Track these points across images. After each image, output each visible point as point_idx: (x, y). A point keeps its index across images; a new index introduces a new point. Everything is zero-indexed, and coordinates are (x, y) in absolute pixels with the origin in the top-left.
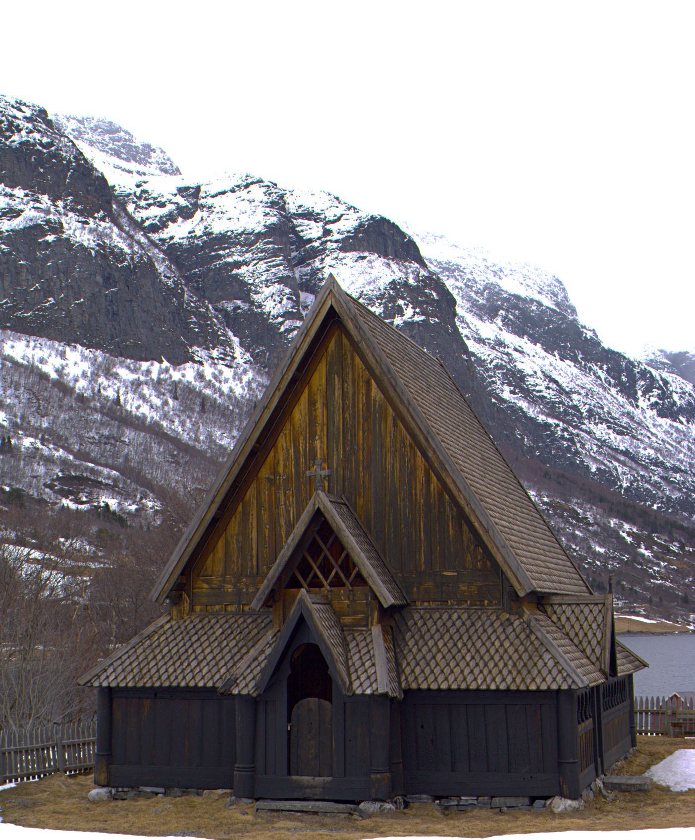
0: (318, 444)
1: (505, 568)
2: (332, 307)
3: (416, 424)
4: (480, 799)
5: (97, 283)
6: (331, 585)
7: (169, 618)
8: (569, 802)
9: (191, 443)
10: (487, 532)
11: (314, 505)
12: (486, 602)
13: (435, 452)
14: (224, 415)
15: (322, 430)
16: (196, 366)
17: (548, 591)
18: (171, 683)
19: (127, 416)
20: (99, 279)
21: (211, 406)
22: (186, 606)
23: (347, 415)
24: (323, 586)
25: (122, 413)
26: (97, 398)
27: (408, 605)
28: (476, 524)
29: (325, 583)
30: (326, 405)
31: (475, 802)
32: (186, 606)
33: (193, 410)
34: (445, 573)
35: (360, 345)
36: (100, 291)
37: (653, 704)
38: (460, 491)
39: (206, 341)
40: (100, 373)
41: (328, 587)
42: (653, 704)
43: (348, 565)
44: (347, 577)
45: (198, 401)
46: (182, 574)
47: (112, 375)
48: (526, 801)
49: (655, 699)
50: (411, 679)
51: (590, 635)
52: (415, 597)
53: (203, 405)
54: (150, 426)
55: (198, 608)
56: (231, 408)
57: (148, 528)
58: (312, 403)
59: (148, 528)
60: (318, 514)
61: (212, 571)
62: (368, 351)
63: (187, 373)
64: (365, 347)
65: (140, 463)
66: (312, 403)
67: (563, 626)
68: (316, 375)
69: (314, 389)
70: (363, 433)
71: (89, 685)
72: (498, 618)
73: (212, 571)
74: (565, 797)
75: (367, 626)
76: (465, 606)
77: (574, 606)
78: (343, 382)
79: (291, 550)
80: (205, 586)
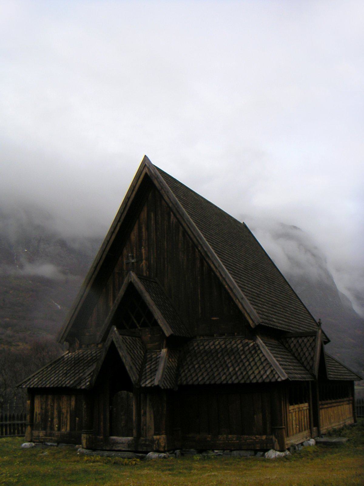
0: (143, 251)
3: (192, 232)
4: (226, 451)
8: (278, 453)
12: (236, 334)
13: (202, 247)
17: (286, 330)
18: (227, 381)
22: (77, 345)
24: (137, 327)
30: (148, 229)
31: (221, 454)
35: (161, 192)
38: (216, 268)
41: (139, 328)
43: (150, 315)
50: (184, 379)
51: (307, 354)
55: (83, 346)
58: (140, 229)
60: (131, 286)
62: (165, 195)
64: (164, 192)
66: (140, 229)
67: (292, 350)
70: (167, 242)
71: (21, 387)
72: (241, 342)
74: (276, 450)
76: (224, 337)
77: (298, 338)
78: (156, 215)
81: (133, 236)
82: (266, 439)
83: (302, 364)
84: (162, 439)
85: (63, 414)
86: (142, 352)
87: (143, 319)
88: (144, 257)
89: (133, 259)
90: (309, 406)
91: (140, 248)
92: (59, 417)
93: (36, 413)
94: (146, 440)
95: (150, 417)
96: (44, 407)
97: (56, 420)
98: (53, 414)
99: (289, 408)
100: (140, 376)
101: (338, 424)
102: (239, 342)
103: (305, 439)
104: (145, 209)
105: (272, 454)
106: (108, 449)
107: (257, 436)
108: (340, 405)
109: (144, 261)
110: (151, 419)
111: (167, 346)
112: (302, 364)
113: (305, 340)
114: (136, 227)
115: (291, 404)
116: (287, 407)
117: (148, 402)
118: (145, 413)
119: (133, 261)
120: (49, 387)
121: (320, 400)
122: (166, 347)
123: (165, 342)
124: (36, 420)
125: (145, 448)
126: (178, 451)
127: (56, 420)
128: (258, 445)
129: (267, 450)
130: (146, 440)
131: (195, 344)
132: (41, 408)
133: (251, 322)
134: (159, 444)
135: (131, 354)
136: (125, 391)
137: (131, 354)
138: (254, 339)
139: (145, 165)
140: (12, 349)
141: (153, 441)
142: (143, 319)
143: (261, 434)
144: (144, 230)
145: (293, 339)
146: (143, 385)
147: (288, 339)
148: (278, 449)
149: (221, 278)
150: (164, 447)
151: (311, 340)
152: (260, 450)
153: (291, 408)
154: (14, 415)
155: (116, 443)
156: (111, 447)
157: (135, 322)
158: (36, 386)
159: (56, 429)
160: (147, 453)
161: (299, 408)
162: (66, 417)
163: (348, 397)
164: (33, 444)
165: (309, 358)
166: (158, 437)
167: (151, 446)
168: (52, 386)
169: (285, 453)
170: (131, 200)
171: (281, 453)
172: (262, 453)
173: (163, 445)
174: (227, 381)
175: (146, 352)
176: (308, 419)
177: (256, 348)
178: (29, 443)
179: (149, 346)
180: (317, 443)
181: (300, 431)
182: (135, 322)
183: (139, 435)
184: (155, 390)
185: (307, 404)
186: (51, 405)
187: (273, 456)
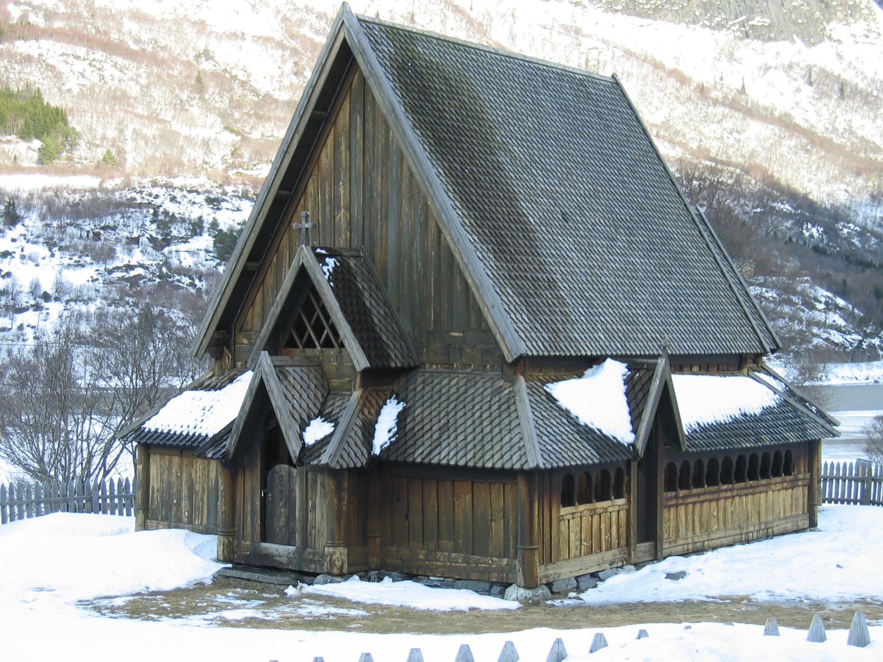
0: (342, 190)
1: (494, 330)
2: (344, 40)
6: (322, 346)
7: (211, 374)
9: (828, 136)
10: (478, 290)
11: (299, 261)
14: (866, 103)
15: (345, 176)
16: (835, 44)
18: (449, 461)
19: (753, 106)
21: (852, 91)
22: (227, 361)
23: (367, 158)
24: (315, 347)
25: (747, 103)
26: (719, 87)
27: (416, 367)
28: (470, 281)
29: (317, 344)
30: (349, 147)
32: (227, 361)
33: (829, 97)
34: (452, 334)
37: (838, 470)
39: (846, 16)
40: (723, 57)
42: (838, 470)
44: (319, 339)
45: (836, 87)
46: (219, 328)
47: (735, 60)
48: (487, 586)
49: (841, 466)
52: (424, 358)
53: (842, 91)
54: (780, 117)
56: (875, 93)
57: (775, 234)
58: (336, 146)
59: (775, 234)
61: (252, 326)
63: (821, 56)
65: (767, 159)
66: (336, 146)
68: (341, 114)
69: (339, 129)
70: (382, 178)
73: (252, 326)
75: (350, 390)
76: (469, 370)
79: (280, 308)
80: (245, 341)
81: (326, 158)
82: (507, 564)
85: (197, 493)
86: (319, 395)
89: (307, 221)
90: (629, 501)
91: (336, 184)
92: (190, 498)
93: (153, 488)
94: (314, 554)
96: (165, 477)
97: (185, 503)
98: (180, 491)
99: (559, 512)
101: (738, 532)
103: (607, 566)
104: (347, 105)
107: (495, 559)
108: (753, 494)
109: (343, 210)
110: (322, 518)
114: (330, 142)
115: (564, 506)
118: (314, 507)
119: (307, 226)
124: (153, 500)
126: (373, 573)
127: (185, 503)
128: (494, 575)
130: (314, 554)
131: (420, 380)
132: (162, 480)
133: (506, 352)
134: (332, 563)
136: (286, 466)
138: (513, 382)
142: (325, 333)
143: (499, 557)
144: (343, 148)
148: (522, 584)
149: (461, 264)
150: (341, 568)
153: (565, 511)
154: (127, 479)
159: (186, 520)
162: (202, 500)
166: (331, 550)
169: (534, 591)
171: (527, 592)
173: (338, 564)
174: (449, 461)
177: (511, 401)
181: (590, 552)
182: (313, 336)
183: (305, 544)
184: (326, 469)
185: (621, 501)
186: (177, 476)
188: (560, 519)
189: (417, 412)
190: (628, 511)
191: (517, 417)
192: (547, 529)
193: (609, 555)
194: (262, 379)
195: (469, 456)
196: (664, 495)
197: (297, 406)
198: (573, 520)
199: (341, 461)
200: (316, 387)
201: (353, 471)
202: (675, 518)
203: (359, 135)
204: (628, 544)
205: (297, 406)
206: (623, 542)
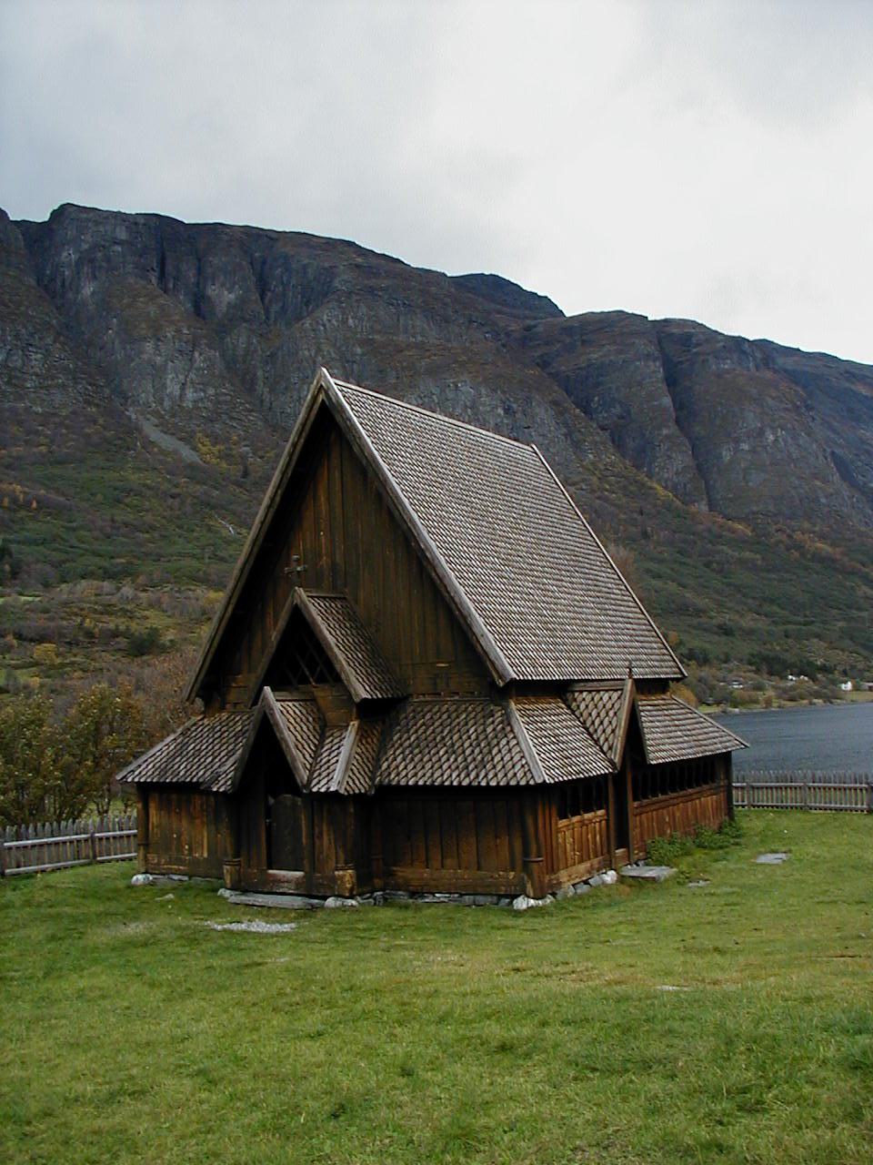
5: (499, 415)
8: (532, 902)
20: (500, 411)
36: (502, 422)
74: (528, 897)
83: (597, 742)
84: (347, 876)
86: (317, 728)
87: (319, 669)
88: (324, 552)
90: (607, 814)
95: (330, 840)
99: (557, 824)
100: (312, 773)
102: (479, 709)
105: (521, 903)
106: (266, 890)
111: (358, 717)
112: (597, 742)
113: (606, 697)
115: (563, 816)
116: (553, 822)
117: (325, 815)
120: (171, 782)
121: (634, 800)
122: (356, 718)
123: (355, 710)
125: (322, 890)
129: (517, 896)
135: (296, 734)
137: (296, 734)
139: (321, 386)
140: (134, 626)
141: (334, 879)
142: (319, 669)
145: (585, 694)
146: (315, 790)
147: (576, 694)
148: (532, 895)
151: (615, 695)
152: (506, 896)
153: (563, 823)
155: (278, 881)
156: (270, 887)
157: (307, 673)
158: (149, 780)
160: (325, 898)
161: (581, 822)
163: (713, 782)
164: (151, 878)
165: (609, 731)
167: (330, 888)
168: (174, 780)
170: (299, 448)
172: (507, 900)
175: (325, 726)
176: (604, 838)
178: (144, 876)
179: (331, 715)
180: (622, 879)
182: (307, 673)
187: (524, 907)
188: (558, 831)
189: (395, 738)
190: (607, 821)
191: (518, 744)
192: (548, 837)
193: (595, 861)
194: (265, 713)
195: (472, 777)
196: (633, 805)
197: (299, 738)
198: (568, 830)
199: (348, 788)
200: (314, 719)
201: (357, 798)
202: (641, 817)
203: (338, 488)
204: (609, 852)
205: (299, 738)
206: (605, 850)
